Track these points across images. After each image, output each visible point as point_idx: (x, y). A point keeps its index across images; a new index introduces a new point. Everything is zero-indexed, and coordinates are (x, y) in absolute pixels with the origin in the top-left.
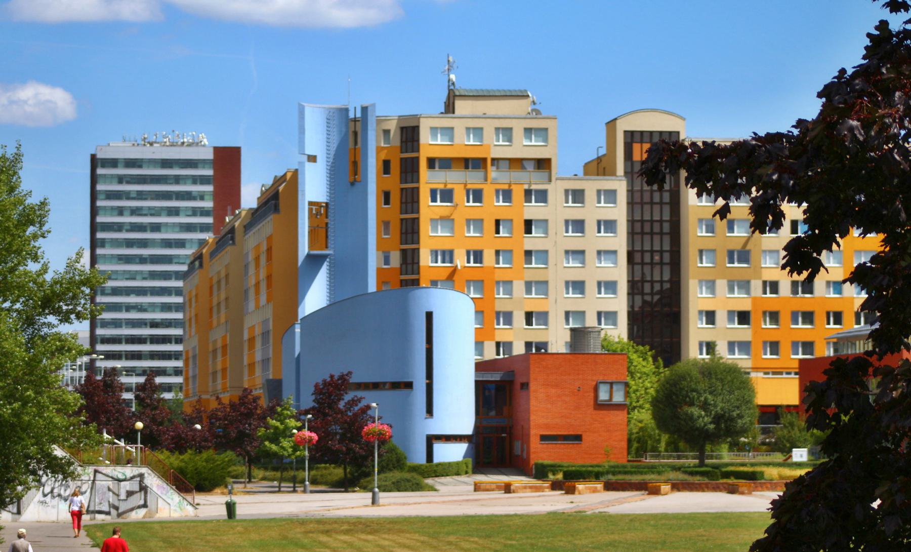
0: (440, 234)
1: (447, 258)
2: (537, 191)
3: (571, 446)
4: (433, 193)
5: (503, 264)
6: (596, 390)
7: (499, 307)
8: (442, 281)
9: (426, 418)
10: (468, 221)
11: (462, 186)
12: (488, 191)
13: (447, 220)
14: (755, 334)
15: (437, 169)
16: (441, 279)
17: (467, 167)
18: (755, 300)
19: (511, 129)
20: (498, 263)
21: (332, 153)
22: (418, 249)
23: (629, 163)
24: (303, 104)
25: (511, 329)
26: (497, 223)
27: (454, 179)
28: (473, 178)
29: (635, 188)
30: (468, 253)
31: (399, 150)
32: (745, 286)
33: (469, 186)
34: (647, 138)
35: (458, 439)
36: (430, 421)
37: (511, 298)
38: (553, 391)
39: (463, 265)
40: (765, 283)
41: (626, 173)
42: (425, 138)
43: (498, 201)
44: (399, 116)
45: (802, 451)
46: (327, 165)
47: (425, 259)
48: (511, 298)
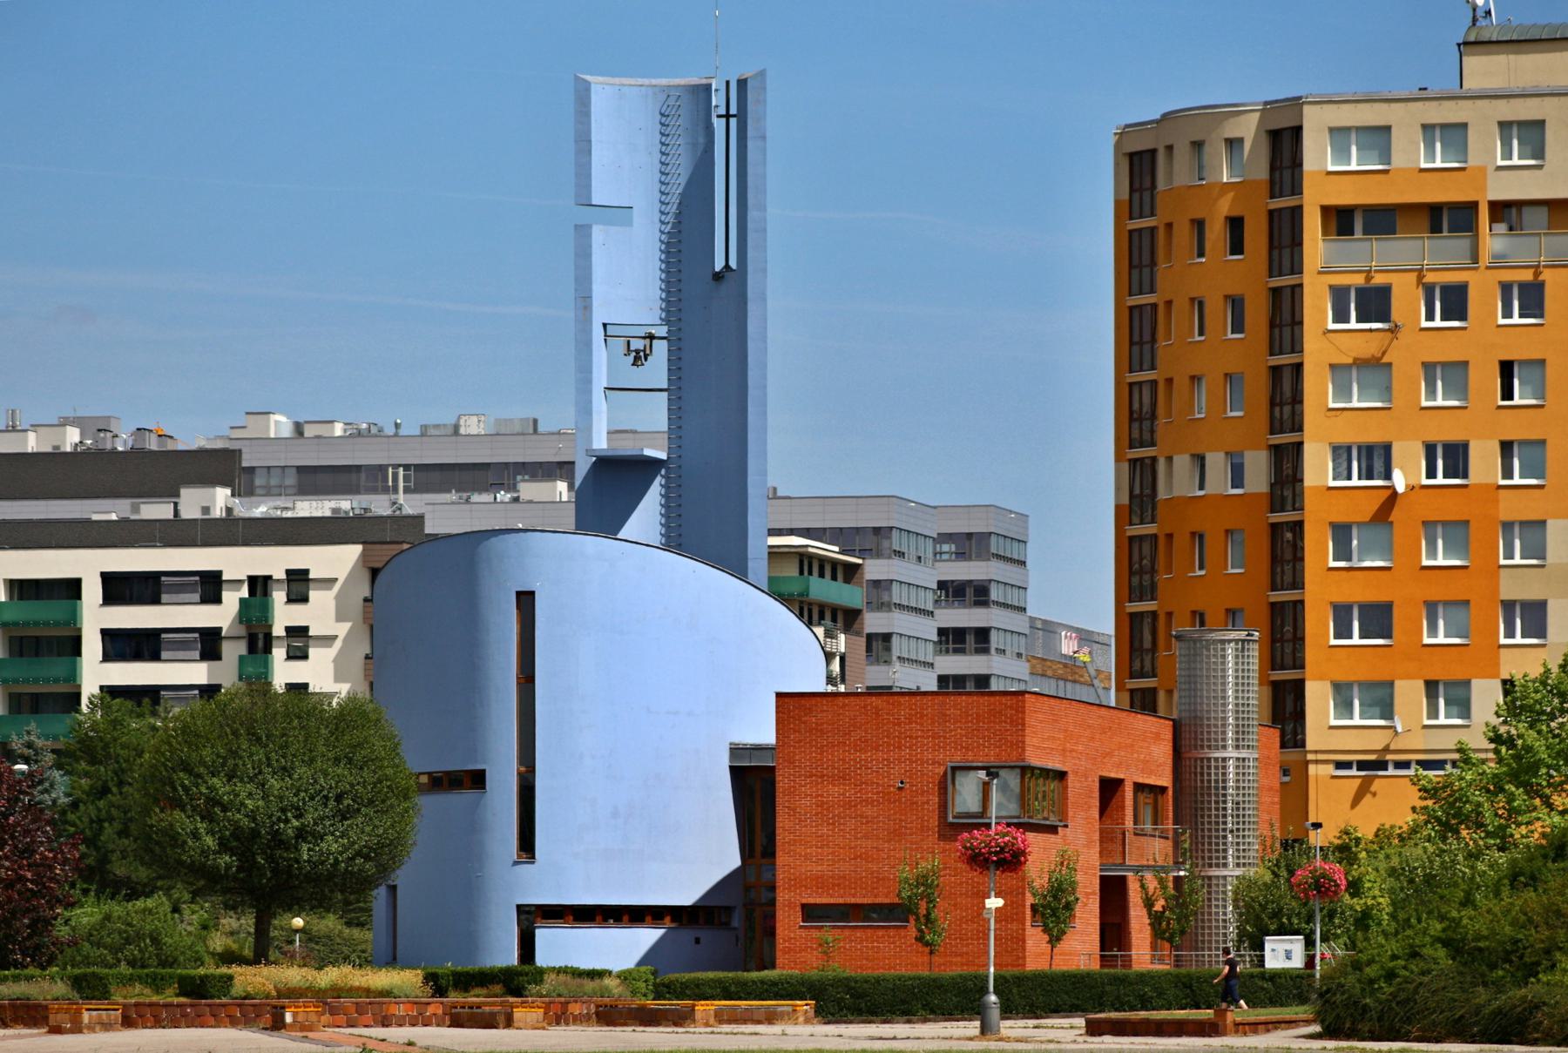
0: (1355, 404)
1: (1378, 465)
3: (880, 933)
4: (1339, 296)
5: (1521, 477)
6: (944, 787)
7: (1510, 589)
8: (1359, 524)
9: (516, 863)
10: (1429, 368)
11: (1413, 277)
13: (1373, 368)
15: (1358, 234)
16: (1359, 519)
17: (1436, 228)
19: (1540, 124)
20: (1508, 474)
21: (674, 200)
22: (1299, 446)
24: (588, 78)
25: (1544, 646)
26: (1507, 369)
30: (1430, 450)
31: (1265, 189)
33: (1430, 278)
35: (598, 918)
36: (525, 869)
37: (1543, 566)
38: (834, 791)
39: (1413, 482)
42: (1318, 156)
43: (1508, 313)
44: (1266, 103)
45: (1291, 941)
46: (662, 232)
47: (1318, 469)
48: (1543, 566)
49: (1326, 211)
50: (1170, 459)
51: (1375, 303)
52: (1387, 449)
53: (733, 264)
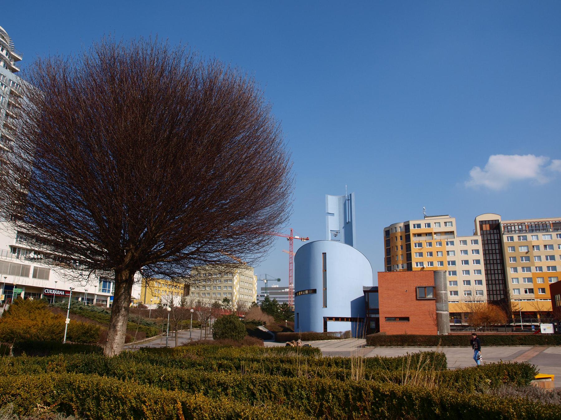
1: (422, 264)
2: (450, 242)
12: (434, 243)
14: (534, 285)
17: (426, 235)
18: (533, 274)
23: (482, 231)
27: (422, 239)
28: (428, 239)
29: (485, 239)
32: (529, 269)
33: (427, 241)
34: (487, 223)
40: (536, 267)
41: (481, 234)
49: (413, 234)
50: (393, 265)
51: (420, 245)
52: (423, 262)
53: (350, 221)
